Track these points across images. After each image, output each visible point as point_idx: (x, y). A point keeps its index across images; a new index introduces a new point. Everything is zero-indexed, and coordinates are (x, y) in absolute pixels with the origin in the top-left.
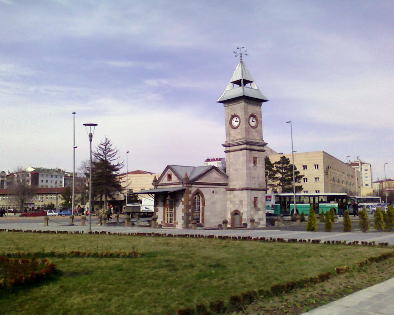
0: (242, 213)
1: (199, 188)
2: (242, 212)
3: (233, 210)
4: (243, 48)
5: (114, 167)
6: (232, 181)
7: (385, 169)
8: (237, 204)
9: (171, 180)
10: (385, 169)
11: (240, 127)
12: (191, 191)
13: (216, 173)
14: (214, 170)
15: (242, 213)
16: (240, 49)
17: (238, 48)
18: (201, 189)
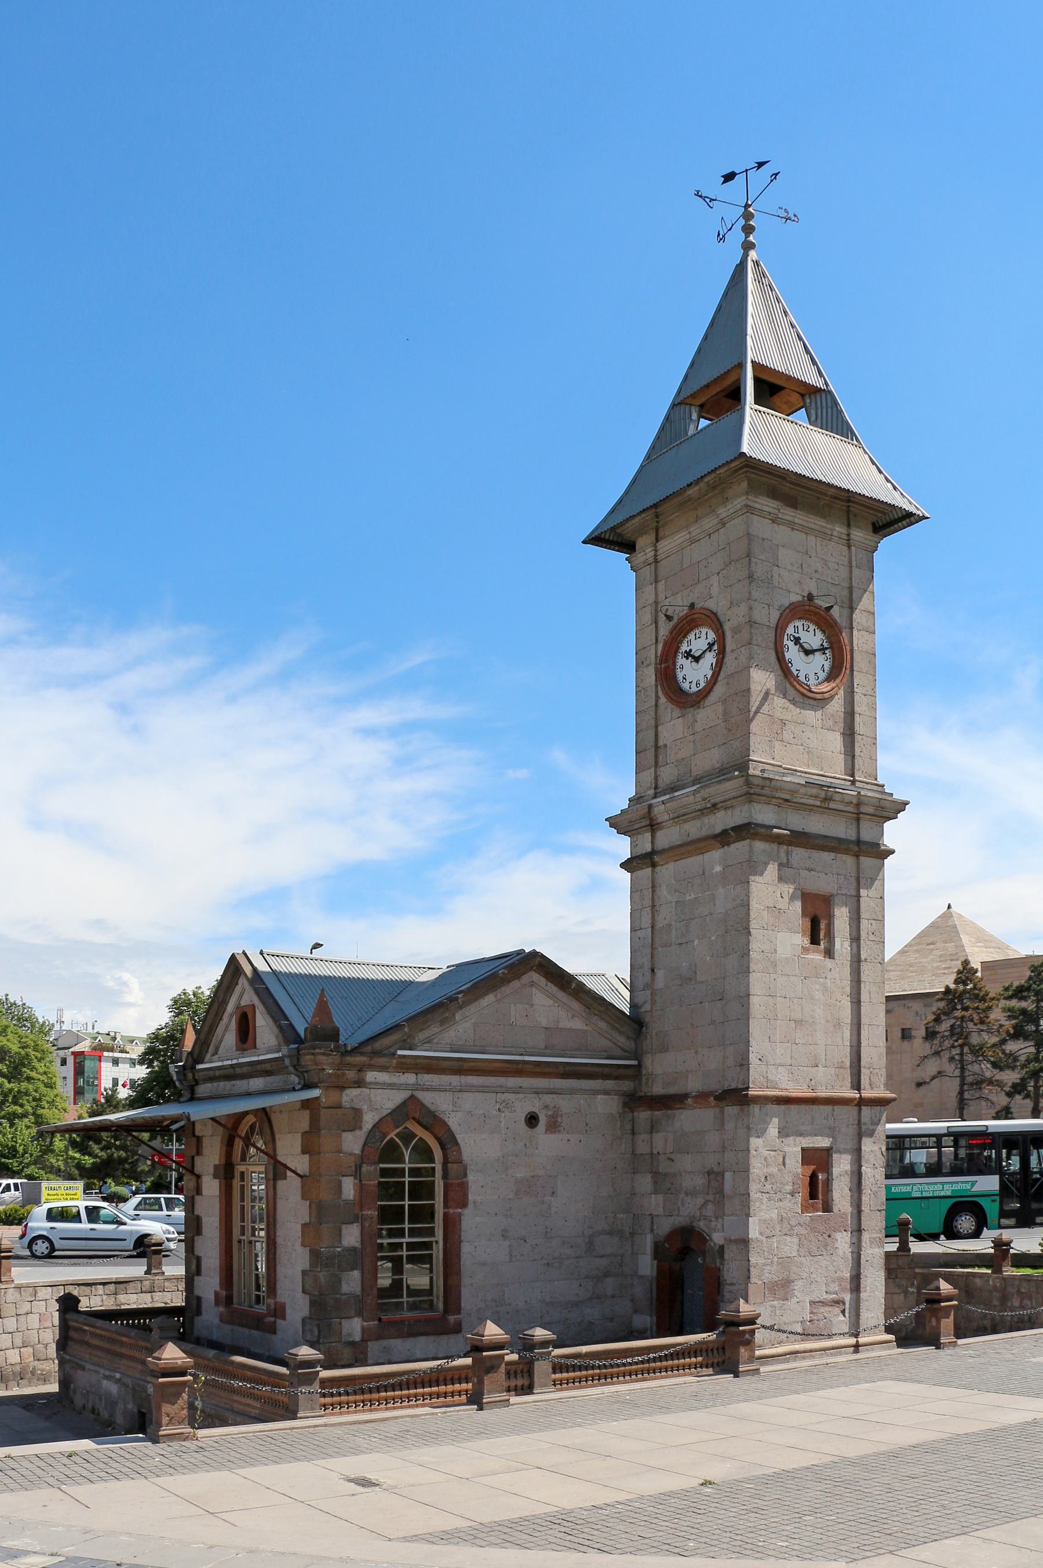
0: (722, 1247)
1: (420, 1095)
2: (721, 1242)
3: (665, 1226)
4: (760, 165)
5: (1017, 1222)
6: (664, 1049)
7: (656, 735)
8: (692, 1193)
9: (254, 1046)
10: (656, 735)
11: (719, 690)
12: (357, 1113)
13: (552, 996)
14: (535, 976)
15: (722, 1247)
16: (740, 179)
17: (729, 177)
18: (437, 1101)
